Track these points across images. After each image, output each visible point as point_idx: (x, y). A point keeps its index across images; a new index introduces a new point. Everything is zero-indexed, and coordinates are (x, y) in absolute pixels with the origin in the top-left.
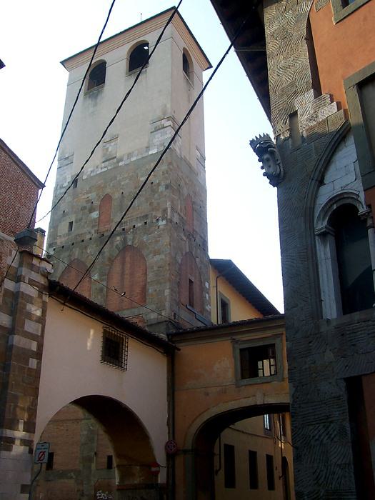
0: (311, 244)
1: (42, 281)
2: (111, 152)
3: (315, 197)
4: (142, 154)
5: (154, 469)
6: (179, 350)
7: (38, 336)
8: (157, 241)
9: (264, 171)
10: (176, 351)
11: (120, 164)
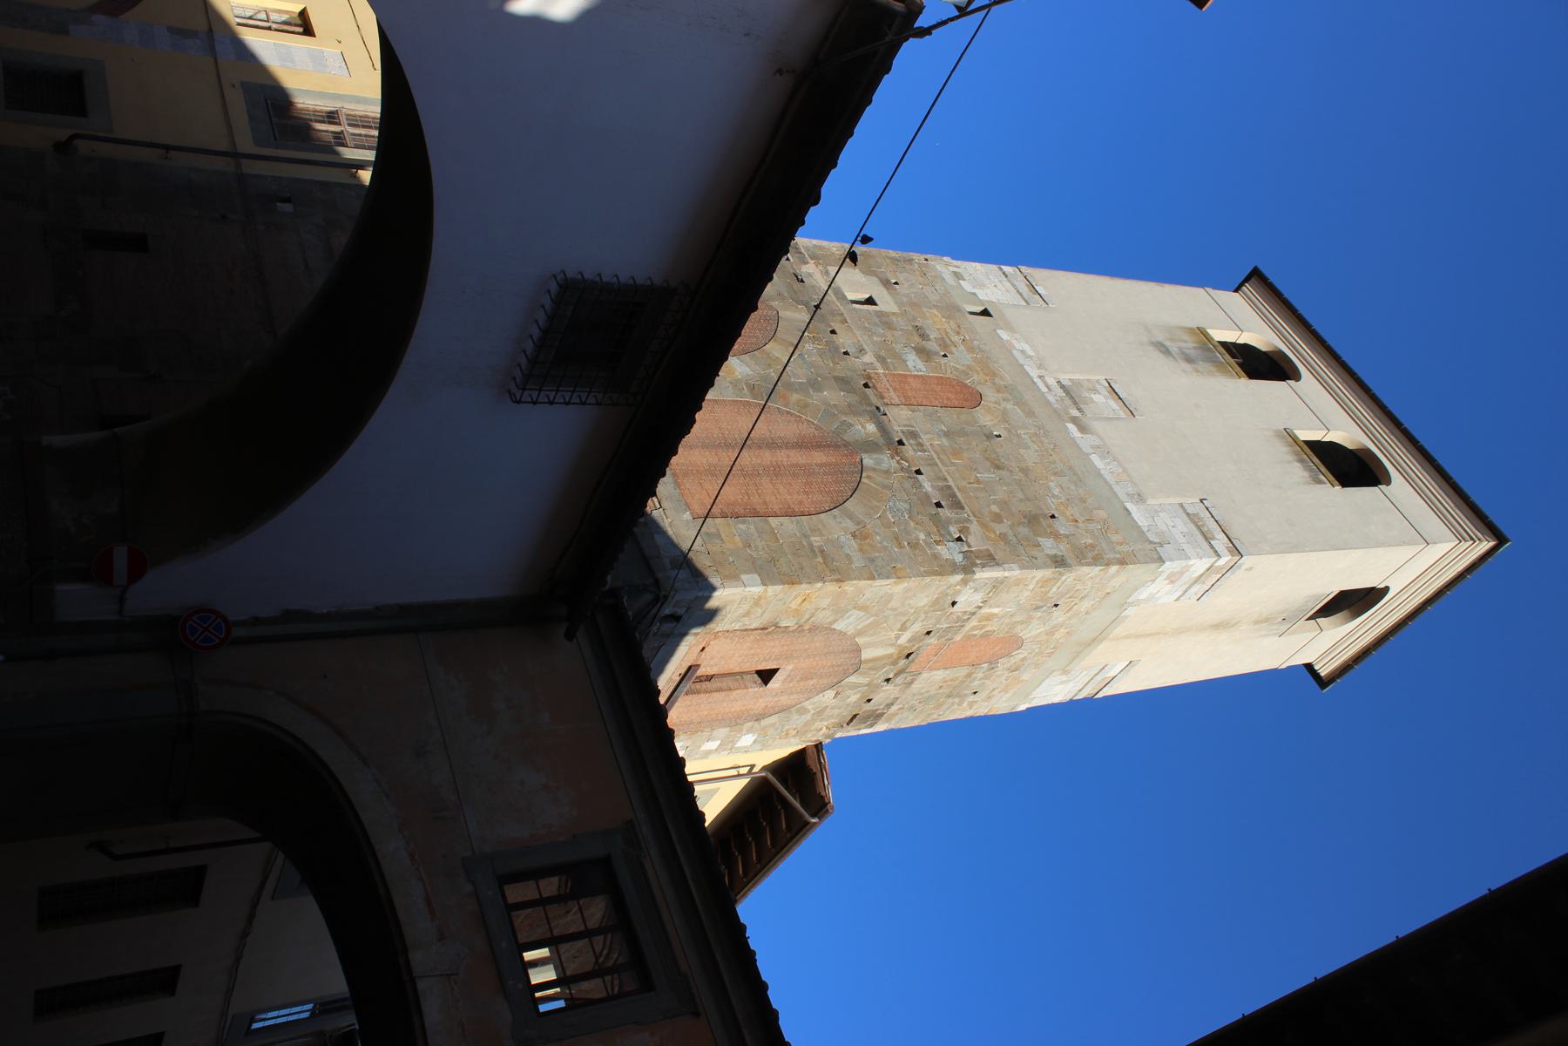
2: (1093, 401)
5: (121, 558)
6: (570, 636)
11: (1071, 426)
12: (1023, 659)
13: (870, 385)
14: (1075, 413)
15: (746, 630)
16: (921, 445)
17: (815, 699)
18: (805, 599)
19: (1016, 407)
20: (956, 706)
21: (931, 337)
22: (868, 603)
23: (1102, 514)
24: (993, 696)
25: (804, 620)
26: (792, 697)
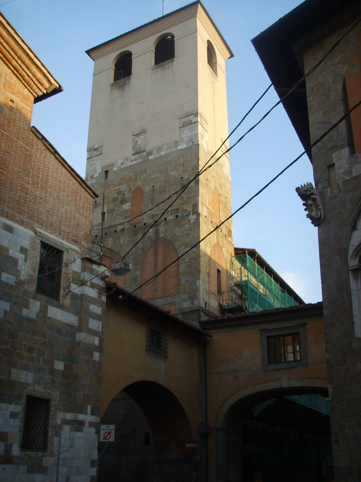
1: (101, 284)
3: (349, 239)
6: (211, 337)
7: (99, 332)
8: (188, 235)
9: (307, 212)
10: (131, 294)
12: (219, 184)
13: (135, 225)
14: (145, 154)
17: (224, 254)
19: (143, 175)
20: (229, 203)
21: (117, 196)
23: (182, 160)
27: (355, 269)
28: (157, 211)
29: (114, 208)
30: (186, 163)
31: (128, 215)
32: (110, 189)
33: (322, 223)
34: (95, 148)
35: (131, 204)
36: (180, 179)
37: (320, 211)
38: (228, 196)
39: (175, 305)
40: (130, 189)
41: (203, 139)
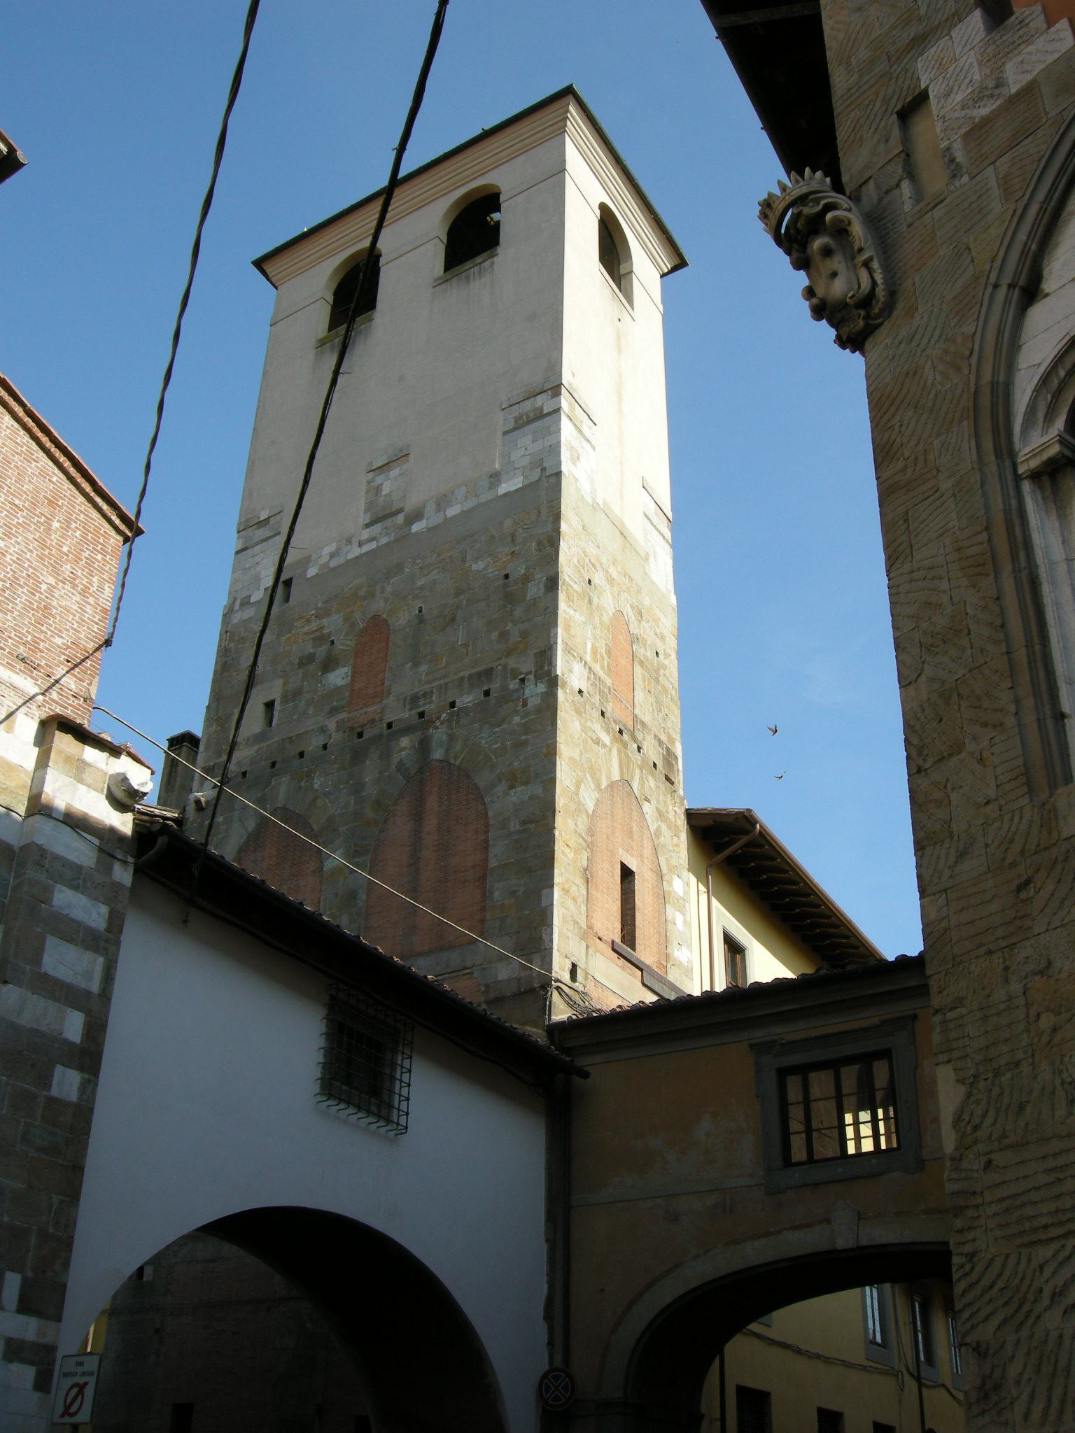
0: (1007, 511)
2: (389, 495)
3: (1010, 345)
4: (477, 496)
6: (586, 1075)
7: (88, 994)
8: (519, 745)
11: (415, 528)
12: (632, 607)
13: (360, 730)
14: (400, 518)
15: (587, 899)
16: (425, 694)
17: (649, 821)
18: (567, 845)
19: (391, 581)
20: (667, 672)
21: (312, 651)
22: (574, 781)
23: (508, 523)
24: (661, 633)
25: (584, 843)
26: (646, 845)
27: (1051, 461)
28: (428, 682)
29: (302, 687)
30: (520, 530)
31: (342, 702)
32: (293, 632)
33: (880, 321)
34: (262, 518)
35: (350, 667)
36: (501, 582)
37: (871, 272)
38: (665, 650)
39: (472, 973)
40: (353, 625)
41: (577, 463)
